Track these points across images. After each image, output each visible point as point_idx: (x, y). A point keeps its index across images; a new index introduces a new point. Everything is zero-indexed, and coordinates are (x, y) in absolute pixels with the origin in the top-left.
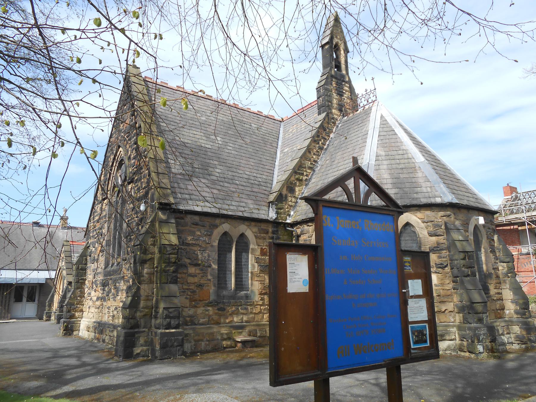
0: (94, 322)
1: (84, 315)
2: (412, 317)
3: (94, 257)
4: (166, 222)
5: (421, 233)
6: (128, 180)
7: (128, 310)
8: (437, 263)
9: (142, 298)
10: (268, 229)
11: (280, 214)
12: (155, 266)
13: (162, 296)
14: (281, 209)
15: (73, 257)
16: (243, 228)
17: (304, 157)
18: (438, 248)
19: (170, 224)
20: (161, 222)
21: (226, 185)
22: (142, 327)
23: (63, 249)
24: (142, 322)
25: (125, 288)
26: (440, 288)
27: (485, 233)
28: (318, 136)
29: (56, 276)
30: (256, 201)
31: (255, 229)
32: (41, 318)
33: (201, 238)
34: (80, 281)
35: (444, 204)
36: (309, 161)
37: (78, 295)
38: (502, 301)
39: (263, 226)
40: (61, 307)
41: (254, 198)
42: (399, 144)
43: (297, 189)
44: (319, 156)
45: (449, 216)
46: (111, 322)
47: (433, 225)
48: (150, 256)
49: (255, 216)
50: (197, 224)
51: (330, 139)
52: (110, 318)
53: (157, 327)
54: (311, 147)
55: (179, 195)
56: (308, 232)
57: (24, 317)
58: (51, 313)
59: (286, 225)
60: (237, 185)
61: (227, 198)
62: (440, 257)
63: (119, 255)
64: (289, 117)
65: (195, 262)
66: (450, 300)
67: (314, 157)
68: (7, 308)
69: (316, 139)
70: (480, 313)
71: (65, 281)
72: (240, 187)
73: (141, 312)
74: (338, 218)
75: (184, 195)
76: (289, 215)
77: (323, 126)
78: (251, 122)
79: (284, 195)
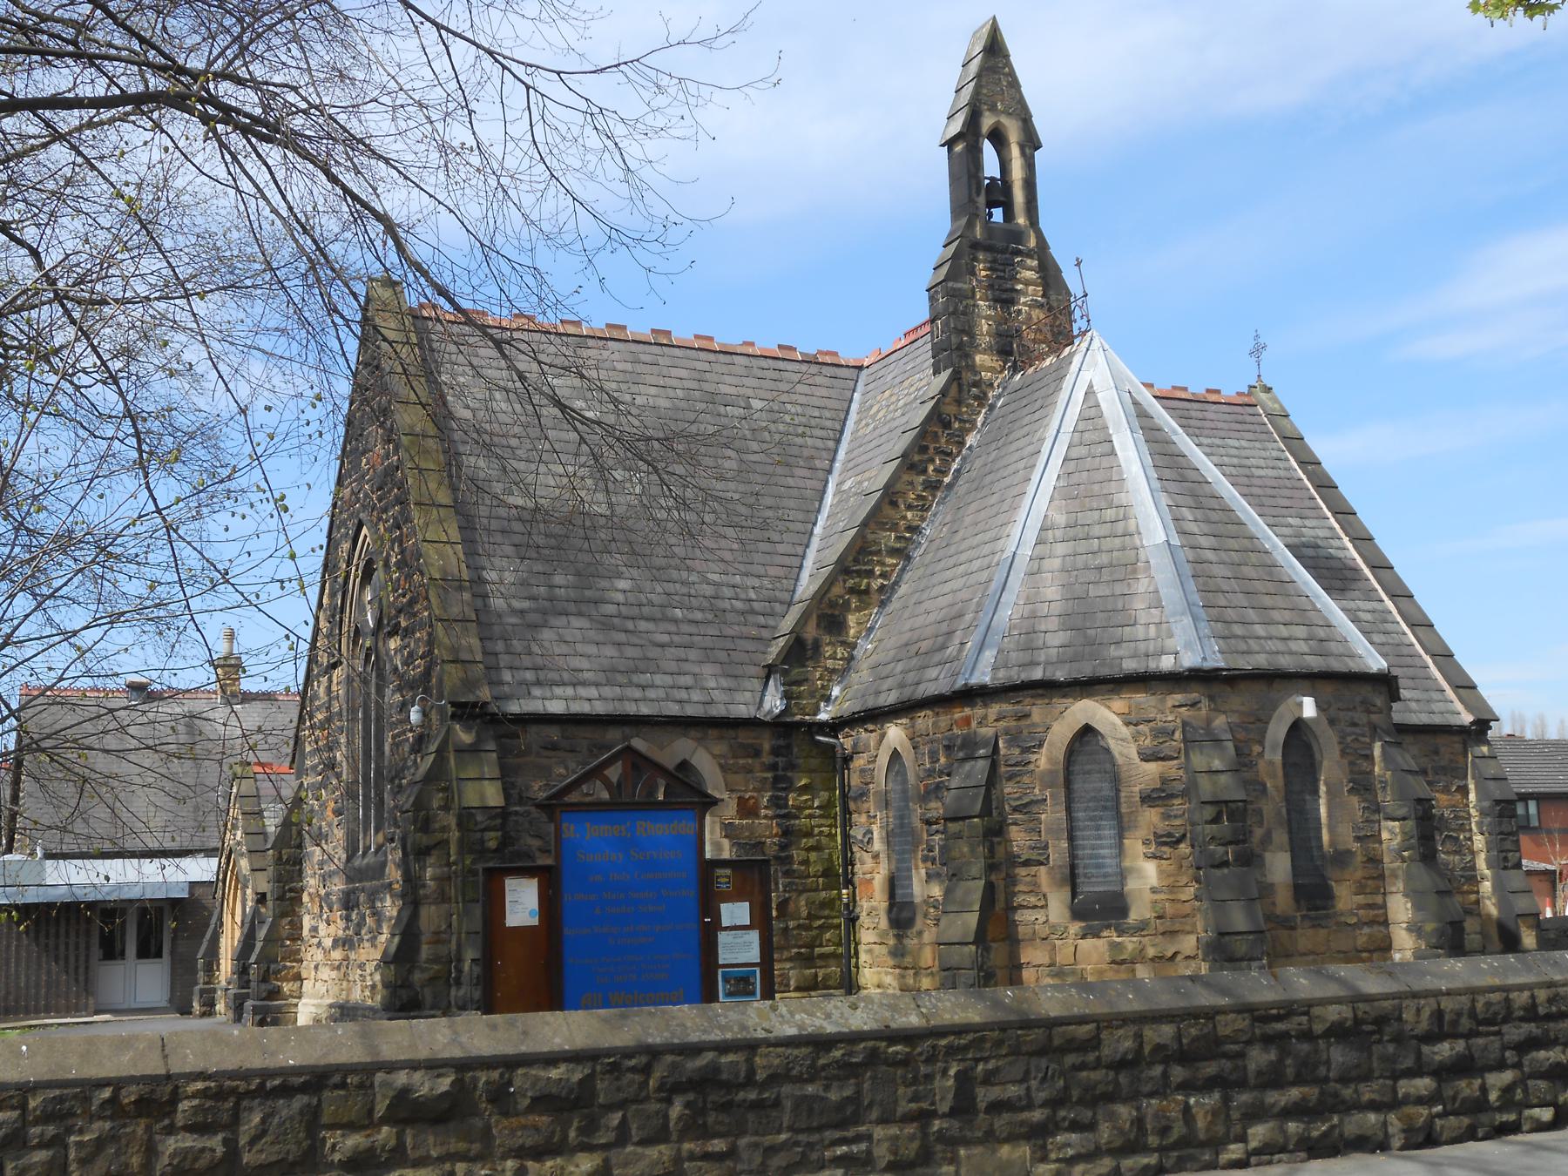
0: (331, 1006)
1: (304, 989)
3: (320, 828)
4: (474, 750)
7: (392, 967)
8: (1158, 831)
9: (424, 938)
10: (761, 745)
11: (798, 698)
13: (468, 933)
14: (799, 683)
16: (682, 748)
17: (874, 520)
18: (1163, 791)
19: (483, 754)
20: (461, 750)
21: (643, 625)
24: (428, 995)
26: (1163, 896)
27: (1335, 740)
28: (924, 450)
30: (731, 671)
31: (720, 748)
32: (185, 1011)
35: (1179, 673)
36: (890, 530)
37: (285, 933)
38: (1382, 929)
39: (745, 737)
40: (242, 970)
41: (722, 656)
43: (852, 619)
45: (1193, 705)
46: (369, 1002)
47: (1151, 731)
49: (718, 711)
50: (554, 747)
51: (964, 451)
52: (367, 993)
53: (460, 1004)
54: (899, 487)
55: (507, 676)
56: (867, 749)
57: (134, 1006)
58: (214, 990)
60: (676, 621)
62: (1166, 817)
64: (884, 353)
66: (1188, 928)
67: (909, 515)
68: (82, 978)
69: (917, 458)
70: (1242, 959)
71: (249, 891)
72: (685, 628)
73: (423, 970)
74: (588, 825)
75: (521, 672)
76: (827, 699)
77: (940, 415)
78: (750, 392)
79: (810, 642)
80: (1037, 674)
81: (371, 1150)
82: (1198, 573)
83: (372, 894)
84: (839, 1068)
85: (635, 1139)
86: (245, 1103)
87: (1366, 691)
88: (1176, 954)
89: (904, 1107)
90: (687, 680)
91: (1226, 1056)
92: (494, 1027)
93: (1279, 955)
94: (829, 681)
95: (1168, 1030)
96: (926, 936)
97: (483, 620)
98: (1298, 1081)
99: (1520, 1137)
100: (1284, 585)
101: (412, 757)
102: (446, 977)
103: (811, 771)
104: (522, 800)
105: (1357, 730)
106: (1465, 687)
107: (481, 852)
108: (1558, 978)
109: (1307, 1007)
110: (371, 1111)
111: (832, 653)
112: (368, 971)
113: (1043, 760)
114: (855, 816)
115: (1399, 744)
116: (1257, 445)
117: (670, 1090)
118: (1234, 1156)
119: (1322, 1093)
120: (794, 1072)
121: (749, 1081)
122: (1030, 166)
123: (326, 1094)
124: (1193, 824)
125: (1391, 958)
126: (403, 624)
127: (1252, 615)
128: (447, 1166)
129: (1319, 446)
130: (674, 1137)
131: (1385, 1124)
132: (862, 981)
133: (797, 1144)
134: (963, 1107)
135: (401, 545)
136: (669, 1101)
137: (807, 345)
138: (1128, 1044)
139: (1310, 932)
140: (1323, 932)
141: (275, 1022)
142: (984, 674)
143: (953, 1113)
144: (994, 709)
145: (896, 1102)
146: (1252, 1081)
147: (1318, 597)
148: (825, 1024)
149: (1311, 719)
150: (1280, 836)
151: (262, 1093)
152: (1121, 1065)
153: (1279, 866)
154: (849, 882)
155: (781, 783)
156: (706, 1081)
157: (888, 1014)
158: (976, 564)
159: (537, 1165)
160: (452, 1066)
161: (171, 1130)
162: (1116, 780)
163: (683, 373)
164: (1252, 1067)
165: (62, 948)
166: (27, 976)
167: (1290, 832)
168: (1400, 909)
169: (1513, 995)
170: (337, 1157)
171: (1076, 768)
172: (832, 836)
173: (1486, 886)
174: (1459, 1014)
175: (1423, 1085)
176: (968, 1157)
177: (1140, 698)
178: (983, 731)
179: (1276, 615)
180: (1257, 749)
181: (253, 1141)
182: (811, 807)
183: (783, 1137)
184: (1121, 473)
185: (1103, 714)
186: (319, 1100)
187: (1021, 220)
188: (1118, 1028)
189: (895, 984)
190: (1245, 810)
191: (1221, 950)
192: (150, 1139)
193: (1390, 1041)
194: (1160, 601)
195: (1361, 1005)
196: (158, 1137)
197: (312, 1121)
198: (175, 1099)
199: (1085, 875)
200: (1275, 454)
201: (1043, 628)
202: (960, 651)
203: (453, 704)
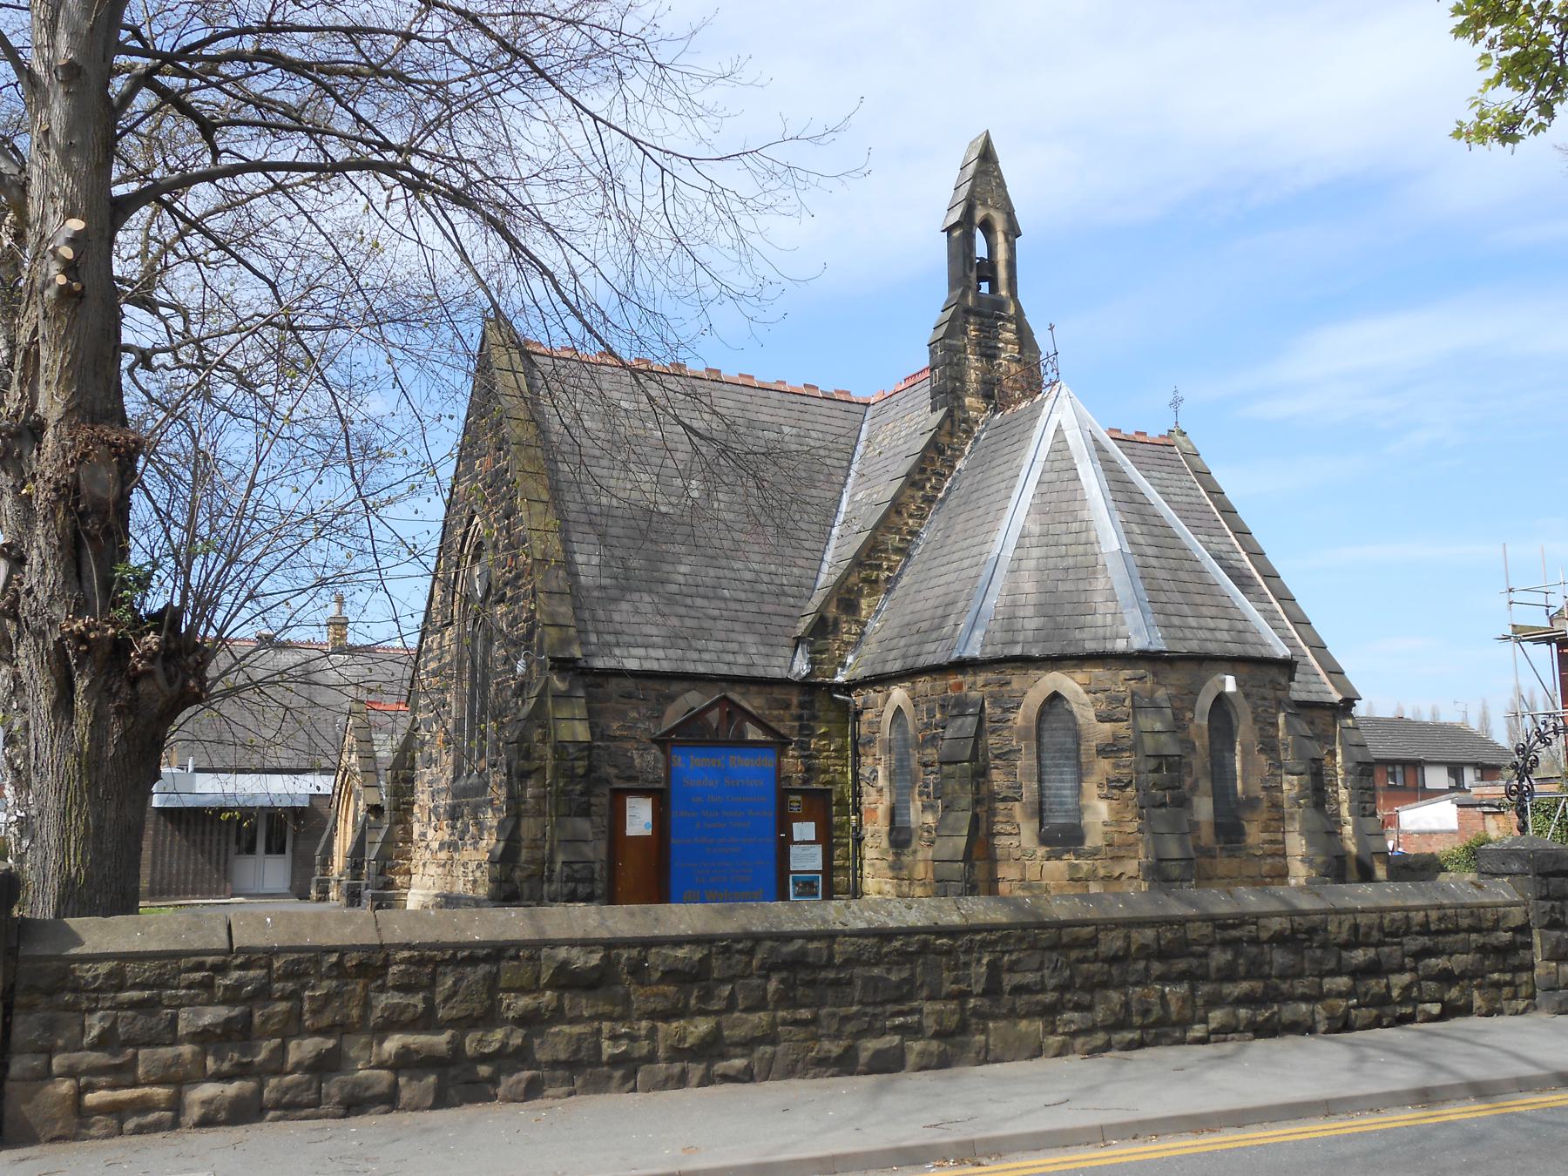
0: (437, 896)
4: (566, 696)
5: (1082, 716)
6: (494, 594)
9: (524, 844)
14: (821, 652)
17: (883, 524)
20: (558, 696)
21: (699, 602)
22: (525, 897)
23: (351, 721)
24: (525, 889)
25: (495, 823)
26: (1113, 829)
27: (1249, 710)
28: (923, 471)
29: (337, 790)
30: (768, 640)
32: (303, 896)
33: (639, 725)
34: (402, 808)
36: (896, 533)
37: (398, 838)
39: (778, 693)
41: (761, 628)
42: (1077, 506)
43: (864, 603)
44: (924, 519)
45: (1140, 679)
46: (470, 894)
49: (758, 672)
50: (629, 696)
51: (954, 473)
52: (469, 886)
54: (903, 499)
55: (593, 638)
56: (875, 705)
57: (262, 892)
58: (329, 881)
59: (833, 688)
60: (725, 599)
62: (1117, 766)
63: (482, 755)
65: (628, 773)
66: (1132, 854)
67: (910, 522)
68: (222, 868)
69: (917, 477)
70: (1175, 880)
71: (361, 803)
72: (733, 605)
73: (523, 869)
76: (843, 665)
78: (782, 420)
80: (1017, 651)
81: (537, 1010)
82: (1144, 573)
84: (899, 955)
85: (741, 1007)
86: (440, 969)
87: (1273, 672)
88: (1121, 874)
89: (949, 987)
90: (734, 646)
91: (1193, 955)
92: (632, 914)
93: (1205, 879)
95: (1149, 934)
96: (921, 858)
97: (575, 593)
98: (1247, 977)
99: (1415, 1026)
100: (1211, 587)
102: (541, 874)
103: (828, 722)
104: (603, 737)
105: (1266, 703)
106: (1335, 672)
107: (572, 777)
108: (1446, 902)
109: (1257, 917)
110: (538, 979)
111: (848, 630)
113: (1019, 718)
114: (863, 758)
115: (1296, 715)
116: (1175, 477)
117: (768, 969)
118: (1198, 1035)
119: (1266, 987)
120: (865, 957)
121: (829, 964)
122: (1012, 250)
123: (504, 964)
124: (1137, 773)
125: (1288, 883)
126: (509, 594)
127: (1186, 610)
128: (596, 1024)
129: (1221, 477)
130: (771, 1006)
131: (1313, 1012)
132: (865, 889)
133: (865, 1014)
134: (992, 989)
135: (508, 532)
136: (767, 978)
137: (826, 386)
138: (1119, 943)
139: (1226, 861)
140: (1236, 861)
141: (389, 907)
142: (974, 649)
143: (985, 993)
144: (981, 678)
145: (941, 983)
146: (1213, 976)
147: (1236, 597)
148: (888, 920)
149: (1232, 693)
150: (1205, 785)
151: (454, 962)
152: (1114, 959)
153: (1204, 808)
154: (857, 811)
155: (806, 730)
156: (797, 963)
157: (935, 914)
158: (967, 563)
159: (665, 1026)
160: (601, 944)
161: (382, 989)
162: (1077, 736)
163: (730, 404)
164: (1213, 964)
165: (207, 843)
166: (178, 865)
167: (1213, 781)
168: (1296, 844)
169: (1412, 914)
170: (511, 1014)
171: (1046, 726)
172: (844, 774)
173: (1348, 830)
174: (1371, 927)
175: (1343, 982)
176: (996, 1029)
177: (1098, 672)
178: (973, 694)
179: (1205, 611)
180: (1189, 715)
181: (446, 1000)
182: (828, 750)
183: (855, 1008)
184: (1084, 495)
185: (1068, 683)
186: (498, 969)
187: (1004, 293)
188: (1112, 930)
189: (892, 891)
190: (1180, 763)
191: (1158, 873)
192: (367, 996)
193: (1318, 947)
194: (1114, 595)
195: (1296, 918)
196: (372, 994)
197: (492, 984)
198: (387, 964)
199: (1051, 810)
200: (1188, 484)
201: (1022, 614)
202: (955, 630)
203: (552, 659)
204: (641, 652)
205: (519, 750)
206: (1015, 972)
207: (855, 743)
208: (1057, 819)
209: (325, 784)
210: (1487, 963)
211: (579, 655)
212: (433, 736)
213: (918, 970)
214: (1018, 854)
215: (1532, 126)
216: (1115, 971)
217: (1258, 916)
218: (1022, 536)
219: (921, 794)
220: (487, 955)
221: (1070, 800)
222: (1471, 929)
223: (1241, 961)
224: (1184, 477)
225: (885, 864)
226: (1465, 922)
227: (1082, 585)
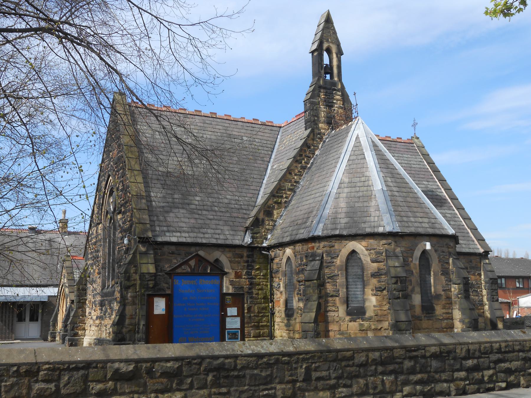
0: (95, 339)
1: (86, 333)
2: (228, 326)
3: (93, 278)
4: (146, 253)
5: (365, 260)
7: (116, 326)
10: (243, 254)
11: (256, 238)
12: (137, 290)
14: (257, 233)
15: (75, 273)
16: (217, 254)
17: (284, 179)
18: (379, 273)
19: (149, 255)
20: (141, 253)
21: (204, 212)
24: (128, 336)
26: (377, 308)
27: (437, 257)
28: (301, 155)
29: (59, 294)
30: (234, 229)
32: (46, 340)
36: (289, 182)
38: (451, 321)
39: (238, 251)
40: (65, 326)
41: (231, 223)
43: (275, 212)
44: (302, 176)
45: (389, 244)
48: (133, 282)
49: (229, 242)
50: (173, 253)
51: (315, 156)
52: (107, 335)
54: (292, 168)
55: (158, 229)
56: (279, 256)
57: (28, 338)
58: (56, 333)
60: (215, 211)
61: (204, 226)
66: (386, 319)
67: (296, 177)
68: (10, 328)
69: (298, 158)
70: (404, 330)
71: (68, 299)
72: (219, 214)
73: (126, 328)
75: (162, 227)
76: (266, 239)
77: (307, 144)
78: (243, 134)
80: (337, 232)
82: (392, 199)
83: (110, 301)
84: (266, 364)
85: (196, 387)
86: (62, 373)
87: (447, 241)
88: (381, 328)
89: (288, 378)
90: (219, 231)
91: (397, 363)
94: (267, 233)
95: (377, 354)
96: (297, 320)
97: (150, 209)
99: (495, 392)
100: (421, 204)
101: (125, 255)
103: (260, 263)
105: (444, 254)
106: (481, 240)
107: (147, 288)
108: (509, 339)
110: (106, 376)
111: (268, 224)
112: (108, 328)
114: (274, 279)
115: (458, 259)
116: (414, 156)
117: (208, 371)
119: (428, 376)
120: (250, 366)
121: (235, 369)
122: (339, 61)
123: (91, 370)
124: (388, 284)
126: (123, 210)
127: (410, 214)
128: (131, 395)
129: (434, 158)
130: (209, 387)
131: (449, 387)
132: (275, 335)
133: (251, 390)
134: (307, 379)
135: (122, 183)
136: (207, 375)
137: (263, 119)
138: (364, 358)
140: (431, 322)
142: (319, 232)
143: (304, 381)
144: (322, 244)
145: (284, 377)
146: (405, 372)
147: (432, 209)
148: (261, 350)
150: (417, 289)
151: (69, 369)
152: (361, 365)
153: (417, 299)
154: (272, 301)
156: (220, 368)
157: (282, 347)
158: (318, 195)
160: (134, 361)
161: (37, 381)
162: (363, 268)
163: (220, 127)
164: (405, 367)
165: (4, 317)
167: (421, 288)
168: (457, 314)
169: (493, 345)
170: (94, 392)
171: (349, 264)
172: (267, 285)
173: (487, 307)
174: (475, 351)
175: (463, 374)
176: (309, 396)
177: (372, 241)
180: (410, 259)
181: (65, 386)
182: (260, 275)
183: (246, 388)
184: (367, 165)
185: (359, 246)
186: (88, 372)
187: (336, 79)
188: (360, 353)
190: (406, 280)
191: (397, 327)
192: (30, 384)
193: (452, 359)
194: (379, 208)
195: (442, 347)
196: (32, 384)
197: (85, 379)
198: (38, 371)
200: (419, 160)
201: (339, 217)
202: (311, 224)
203: (139, 238)
204: (178, 234)
205: (125, 277)
206: (317, 371)
207: (271, 272)
208: (354, 305)
209: (52, 291)
210: (527, 365)
211: (151, 236)
212: (94, 271)
213: (274, 371)
214: (337, 319)
215: (517, 9)
216: (362, 370)
217: (425, 346)
218: (340, 183)
219: (298, 294)
220: (84, 366)
221: (359, 296)
222: (519, 351)
223: (418, 365)
224: (418, 157)
225: (283, 324)
226: (517, 348)
227: (365, 204)
